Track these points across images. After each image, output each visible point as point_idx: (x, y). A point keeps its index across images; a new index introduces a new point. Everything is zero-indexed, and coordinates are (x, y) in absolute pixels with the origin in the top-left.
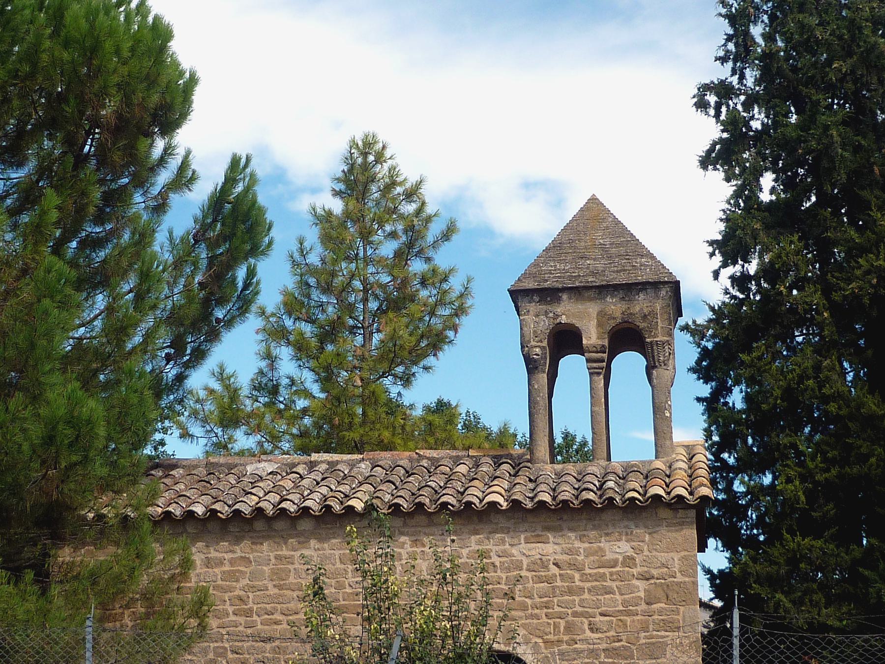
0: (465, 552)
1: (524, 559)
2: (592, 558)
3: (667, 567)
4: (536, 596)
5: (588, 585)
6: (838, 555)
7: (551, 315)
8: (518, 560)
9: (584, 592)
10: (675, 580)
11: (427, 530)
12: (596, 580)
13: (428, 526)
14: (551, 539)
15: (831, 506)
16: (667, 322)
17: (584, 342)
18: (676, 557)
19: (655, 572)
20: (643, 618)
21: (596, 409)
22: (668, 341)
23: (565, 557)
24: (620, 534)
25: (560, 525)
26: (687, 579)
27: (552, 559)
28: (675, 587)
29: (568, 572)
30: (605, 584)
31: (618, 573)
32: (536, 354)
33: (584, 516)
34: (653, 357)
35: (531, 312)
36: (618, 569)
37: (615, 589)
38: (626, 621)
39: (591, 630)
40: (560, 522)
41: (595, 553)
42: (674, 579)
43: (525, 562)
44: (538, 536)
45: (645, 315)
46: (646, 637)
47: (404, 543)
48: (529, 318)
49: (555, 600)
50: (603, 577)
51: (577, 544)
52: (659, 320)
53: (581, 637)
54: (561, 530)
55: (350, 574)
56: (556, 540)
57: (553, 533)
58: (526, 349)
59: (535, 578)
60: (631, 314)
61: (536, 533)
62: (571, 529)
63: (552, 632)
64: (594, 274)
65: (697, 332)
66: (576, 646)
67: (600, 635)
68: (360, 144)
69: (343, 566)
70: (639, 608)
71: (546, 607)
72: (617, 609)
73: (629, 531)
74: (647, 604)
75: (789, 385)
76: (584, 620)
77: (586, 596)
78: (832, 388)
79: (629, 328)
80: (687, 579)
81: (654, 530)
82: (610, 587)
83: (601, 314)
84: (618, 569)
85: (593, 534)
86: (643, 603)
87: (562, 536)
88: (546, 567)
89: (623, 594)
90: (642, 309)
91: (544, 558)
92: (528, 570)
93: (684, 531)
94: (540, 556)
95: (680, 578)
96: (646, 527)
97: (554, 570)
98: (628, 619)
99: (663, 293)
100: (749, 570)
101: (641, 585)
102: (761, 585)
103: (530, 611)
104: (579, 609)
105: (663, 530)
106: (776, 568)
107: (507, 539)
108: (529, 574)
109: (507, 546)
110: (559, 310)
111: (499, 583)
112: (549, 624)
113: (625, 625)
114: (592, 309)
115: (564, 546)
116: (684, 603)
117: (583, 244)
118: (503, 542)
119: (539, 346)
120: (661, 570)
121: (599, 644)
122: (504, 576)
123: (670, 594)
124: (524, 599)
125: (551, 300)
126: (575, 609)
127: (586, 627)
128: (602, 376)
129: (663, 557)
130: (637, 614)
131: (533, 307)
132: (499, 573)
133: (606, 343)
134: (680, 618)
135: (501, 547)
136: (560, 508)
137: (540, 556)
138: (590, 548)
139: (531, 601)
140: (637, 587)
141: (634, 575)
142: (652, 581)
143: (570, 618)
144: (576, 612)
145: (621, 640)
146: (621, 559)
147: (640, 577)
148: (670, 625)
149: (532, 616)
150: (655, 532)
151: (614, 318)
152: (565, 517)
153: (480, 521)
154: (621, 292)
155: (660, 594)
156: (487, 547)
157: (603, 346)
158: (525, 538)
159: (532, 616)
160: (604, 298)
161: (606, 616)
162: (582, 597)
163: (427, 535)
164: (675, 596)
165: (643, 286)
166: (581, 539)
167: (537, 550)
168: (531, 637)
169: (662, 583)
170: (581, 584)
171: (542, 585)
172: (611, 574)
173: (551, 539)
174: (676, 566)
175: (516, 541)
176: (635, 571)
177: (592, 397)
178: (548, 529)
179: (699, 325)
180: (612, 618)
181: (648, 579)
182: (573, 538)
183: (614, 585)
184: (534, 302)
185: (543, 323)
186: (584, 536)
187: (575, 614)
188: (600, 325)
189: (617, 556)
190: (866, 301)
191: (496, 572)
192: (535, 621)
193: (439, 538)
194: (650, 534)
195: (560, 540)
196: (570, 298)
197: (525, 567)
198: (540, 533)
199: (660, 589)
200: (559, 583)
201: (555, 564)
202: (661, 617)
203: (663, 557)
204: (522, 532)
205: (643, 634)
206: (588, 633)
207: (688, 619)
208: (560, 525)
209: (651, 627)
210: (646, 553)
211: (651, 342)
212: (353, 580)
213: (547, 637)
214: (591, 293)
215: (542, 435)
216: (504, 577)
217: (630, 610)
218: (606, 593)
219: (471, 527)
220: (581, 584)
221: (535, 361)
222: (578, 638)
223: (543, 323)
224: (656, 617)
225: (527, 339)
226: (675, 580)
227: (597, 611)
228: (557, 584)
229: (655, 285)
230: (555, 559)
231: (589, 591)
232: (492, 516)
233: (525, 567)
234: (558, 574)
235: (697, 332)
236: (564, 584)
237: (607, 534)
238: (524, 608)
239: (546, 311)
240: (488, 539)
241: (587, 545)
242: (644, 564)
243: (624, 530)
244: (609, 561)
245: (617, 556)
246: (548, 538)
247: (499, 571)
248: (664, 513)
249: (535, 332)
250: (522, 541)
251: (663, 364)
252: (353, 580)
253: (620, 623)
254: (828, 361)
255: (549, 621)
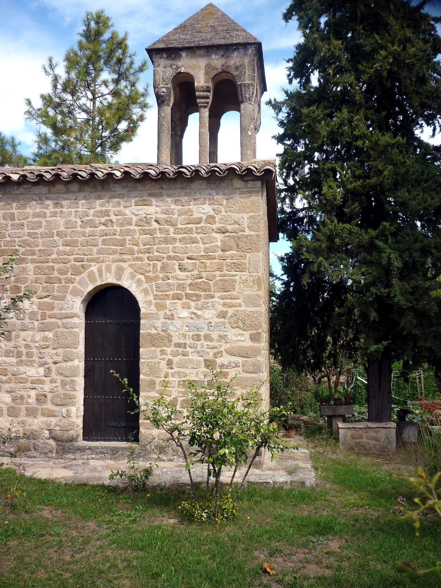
0: (91, 212)
1: (133, 217)
2: (183, 217)
3: (238, 224)
4: (141, 244)
5: (179, 236)
6: (361, 234)
7: (174, 67)
8: (129, 218)
9: (176, 241)
10: (244, 233)
11: (65, 196)
12: (185, 233)
13: (66, 193)
14: (154, 203)
15: (357, 204)
16: (252, 72)
17: (196, 84)
18: (246, 216)
19: (229, 228)
20: (219, 261)
21: (203, 130)
22: (252, 84)
23: (164, 216)
24: (205, 199)
25: (161, 193)
26: (253, 233)
27: (154, 217)
28: (244, 239)
29: (166, 227)
30: (192, 235)
31: (201, 228)
32: (163, 92)
33: (179, 185)
34: (242, 95)
35: (161, 65)
36: (202, 225)
37: (199, 239)
38: (206, 263)
39: (180, 269)
40: (161, 190)
41: (186, 213)
42: (242, 233)
43: (135, 219)
44: (144, 200)
45: (237, 67)
46: (220, 276)
47: (48, 205)
48: (160, 69)
49: (155, 247)
50: (190, 230)
51: (173, 206)
52: (247, 70)
53: (172, 274)
54: (161, 195)
55: (10, 228)
56: (157, 204)
57: (156, 199)
58: (157, 89)
59: (141, 231)
60: (228, 66)
61: (143, 199)
62: (169, 196)
63: (152, 270)
64: (203, 40)
65: (277, 106)
66: (168, 281)
67: (187, 273)
68: (95, 16)
69: (5, 222)
70: (216, 254)
71: (148, 253)
72: (200, 254)
73: (211, 197)
74: (223, 251)
75: (332, 129)
76: (176, 262)
77: (178, 244)
78: (359, 131)
79: (228, 80)
80: (253, 233)
81: (230, 197)
82: (195, 238)
83: (208, 66)
84: (202, 225)
85: (184, 199)
86: (219, 250)
87: (162, 200)
88: (148, 223)
89: (205, 243)
90: (235, 63)
91: (148, 217)
92: (136, 225)
93: (252, 198)
94: (145, 215)
95: (247, 232)
96: (224, 194)
97: (155, 225)
98: (208, 262)
99: (250, 51)
100: (302, 243)
101: (219, 237)
102: (309, 253)
103: (136, 255)
104: (172, 254)
105: (237, 197)
106: (319, 243)
107: (122, 203)
108: (137, 228)
109: (122, 208)
110: (180, 64)
111: (115, 235)
112: (149, 265)
113: (206, 266)
114: (202, 62)
115: (163, 208)
116: (250, 251)
117: (200, 26)
118: (119, 204)
119: (165, 87)
120: (234, 226)
121: (186, 280)
122: (118, 229)
123: (240, 243)
124: (132, 246)
125: (175, 57)
126: (169, 254)
127: (176, 267)
128: (207, 109)
129: (236, 216)
130: (215, 259)
131: (163, 62)
132: (115, 227)
133: (210, 85)
134: (246, 261)
135: (118, 209)
136: (159, 178)
137: (145, 215)
138: (182, 209)
139: (137, 248)
140: (216, 238)
141: (213, 230)
142: (227, 234)
143: (165, 261)
144: (170, 256)
145: (202, 278)
146: (204, 217)
147: (218, 231)
148: (239, 267)
149: (138, 259)
150: (230, 198)
151: (216, 69)
152: (165, 186)
153: (103, 189)
154: (222, 51)
155: (232, 243)
156: (107, 208)
157: (208, 87)
158: (136, 202)
159: (138, 259)
160: (210, 56)
161: (192, 259)
162: (175, 245)
163: (65, 199)
164: (244, 245)
165: (236, 46)
166: (176, 202)
167: (143, 210)
168: (136, 274)
169: (234, 236)
170: (175, 236)
171: (146, 236)
172: (197, 228)
173: (154, 203)
174: (245, 223)
175: (128, 204)
176: (214, 227)
177: (200, 123)
178: (151, 195)
179: (278, 102)
180: (196, 261)
181: (224, 233)
182: (170, 202)
183: (199, 236)
184: (163, 58)
185: (168, 72)
186: (178, 200)
187: (169, 258)
188: (206, 73)
189: (201, 215)
190: (385, 74)
191: (113, 226)
192: (140, 262)
193: (73, 201)
194: (227, 199)
195: (160, 204)
196: (187, 55)
197: (134, 223)
198: (146, 198)
199: (232, 240)
200: (158, 235)
201: (156, 221)
202: (233, 261)
203: (236, 216)
204: (133, 197)
205: (218, 273)
206: (178, 272)
207: (252, 263)
208: (161, 193)
209: (225, 268)
210: (223, 213)
211: (241, 84)
212: (12, 231)
213: (148, 274)
214: (202, 52)
215: (165, 147)
216: (119, 230)
217: (210, 255)
218: (193, 243)
219: (97, 194)
220: (175, 236)
221: (162, 96)
222: (171, 275)
223: (168, 72)
224: (229, 260)
225: (157, 83)
226: (244, 233)
227: (185, 256)
228: (157, 236)
229: (245, 45)
230: (156, 217)
231: (180, 241)
232: (112, 184)
233: (134, 223)
234: (158, 229)
235: (277, 106)
236: (161, 235)
237: (195, 200)
238: (132, 253)
239: (171, 65)
240: (108, 202)
241: (180, 207)
242: (221, 221)
243: (208, 197)
244: (195, 219)
245: (201, 215)
246: (152, 202)
247: (115, 226)
248: (238, 183)
249: (163, 78)
250: (133, 204)
251: (248, 100)
252: (12, 231)
253: (202, 265)
254: (358, 117)
255: (150, 262)
